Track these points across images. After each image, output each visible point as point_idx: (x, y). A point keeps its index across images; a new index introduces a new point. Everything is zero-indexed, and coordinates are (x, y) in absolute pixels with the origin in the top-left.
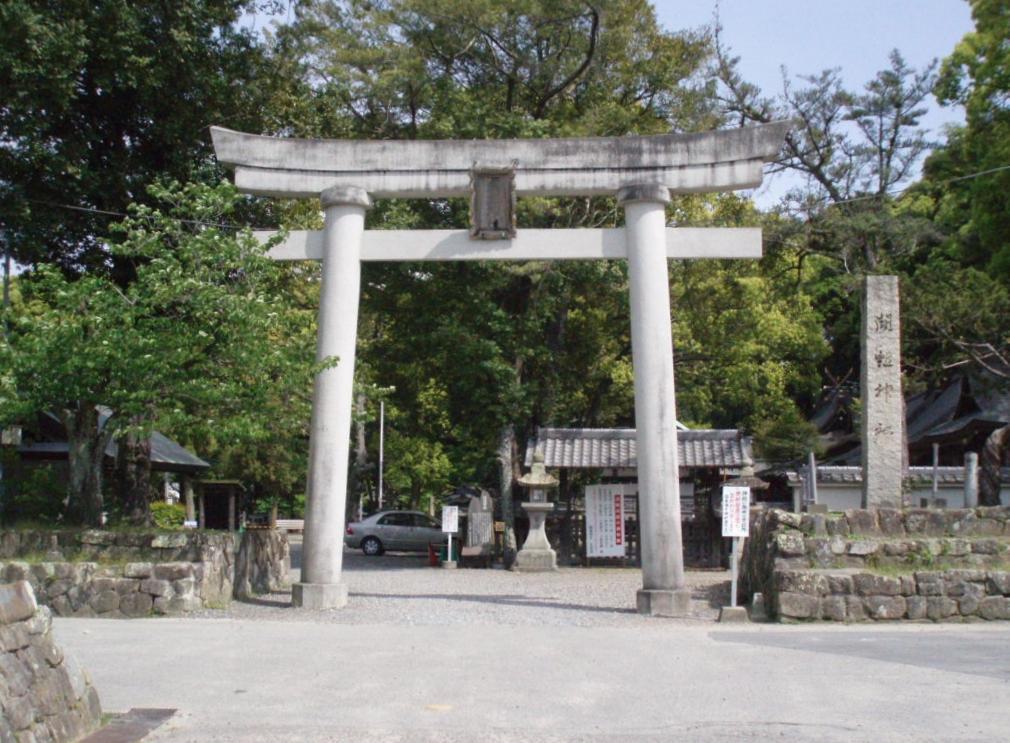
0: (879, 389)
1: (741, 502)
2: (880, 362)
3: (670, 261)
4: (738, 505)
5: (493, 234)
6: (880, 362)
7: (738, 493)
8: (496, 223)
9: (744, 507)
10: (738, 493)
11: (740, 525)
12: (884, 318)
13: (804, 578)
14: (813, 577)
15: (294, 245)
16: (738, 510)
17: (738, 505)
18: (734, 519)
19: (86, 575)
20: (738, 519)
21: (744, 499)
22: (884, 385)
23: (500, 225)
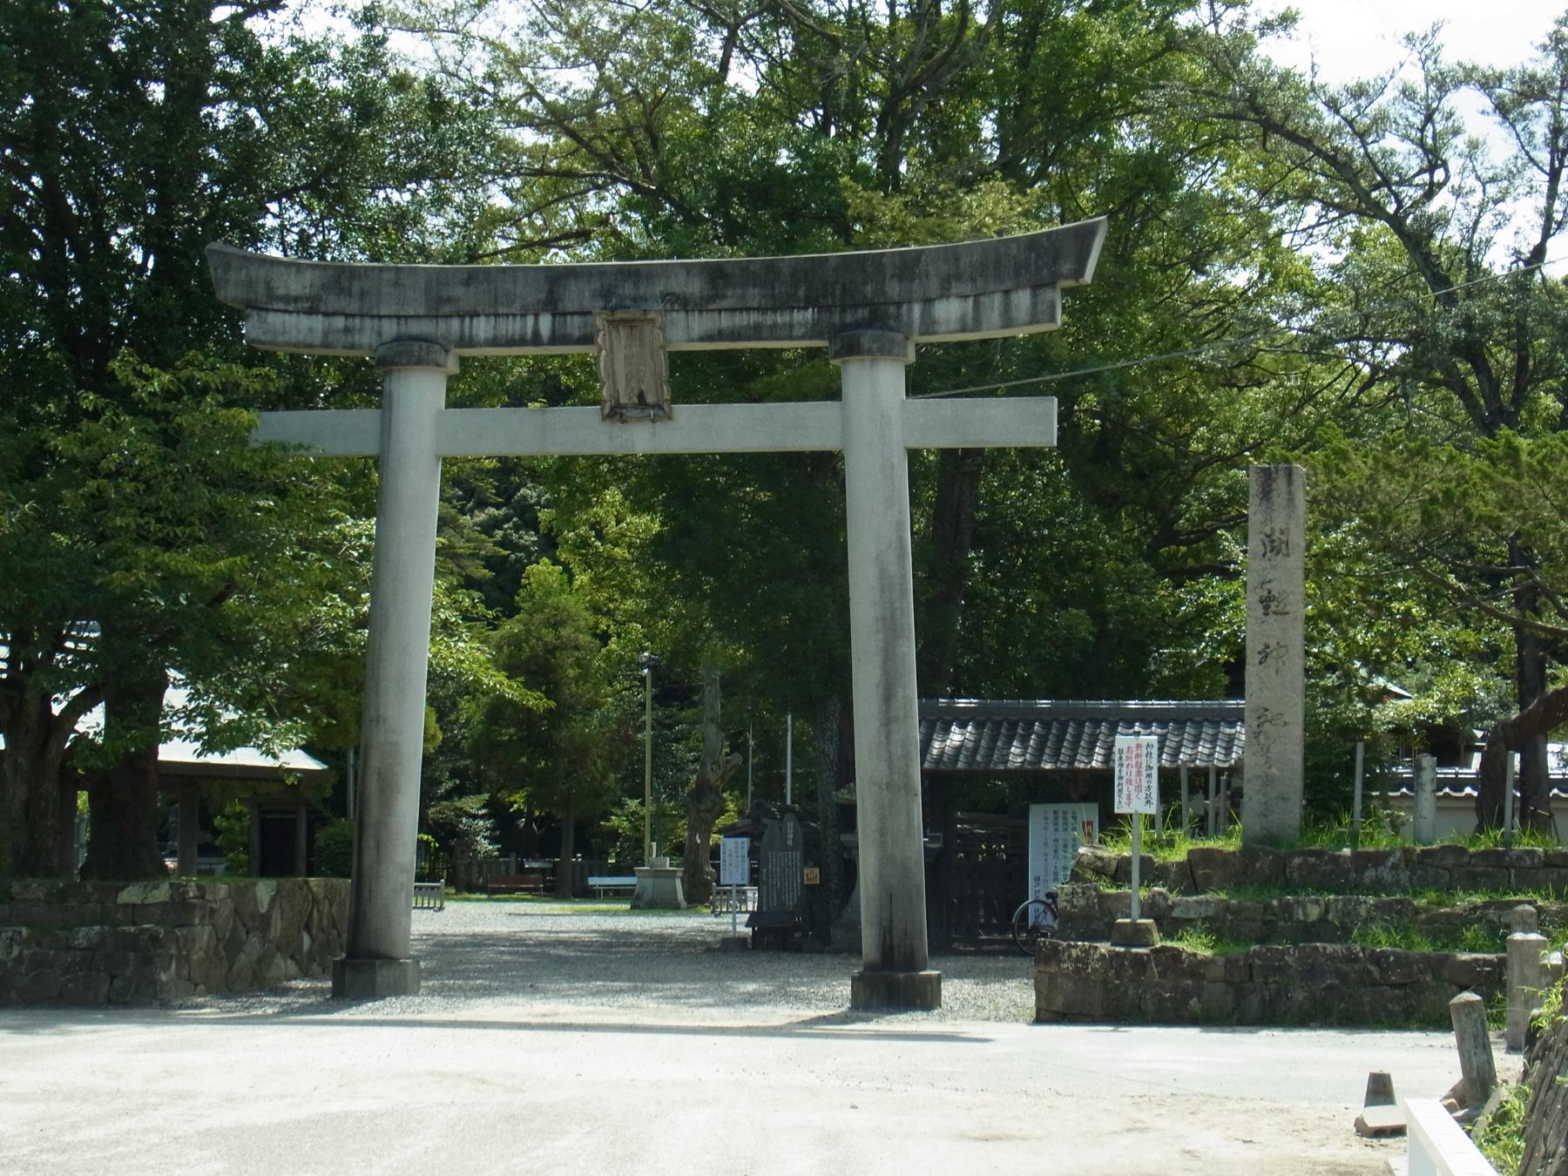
0: (1265, 655)
1: (1144, 759)
2: (1266, 608)
3: (914, 455)
4: (1139, 765)
5: (637, 413)
6: (1266, 608)
7: (1138, 746)
8: (641, 396)
9: (1150, 768)
10: (1138, 746)
11: (1143, 795)
12: (1277, 534)
13: (1074, 952)
14: (1086, 951)
15: (330, 431)
16: (1139, 773)
17: (1139, 765)
18: (1132, 788)
19: (11, 946)
20: (1139, 788)
21: (1149, 755)
22: (1273, 644)
23: (650, 399)
